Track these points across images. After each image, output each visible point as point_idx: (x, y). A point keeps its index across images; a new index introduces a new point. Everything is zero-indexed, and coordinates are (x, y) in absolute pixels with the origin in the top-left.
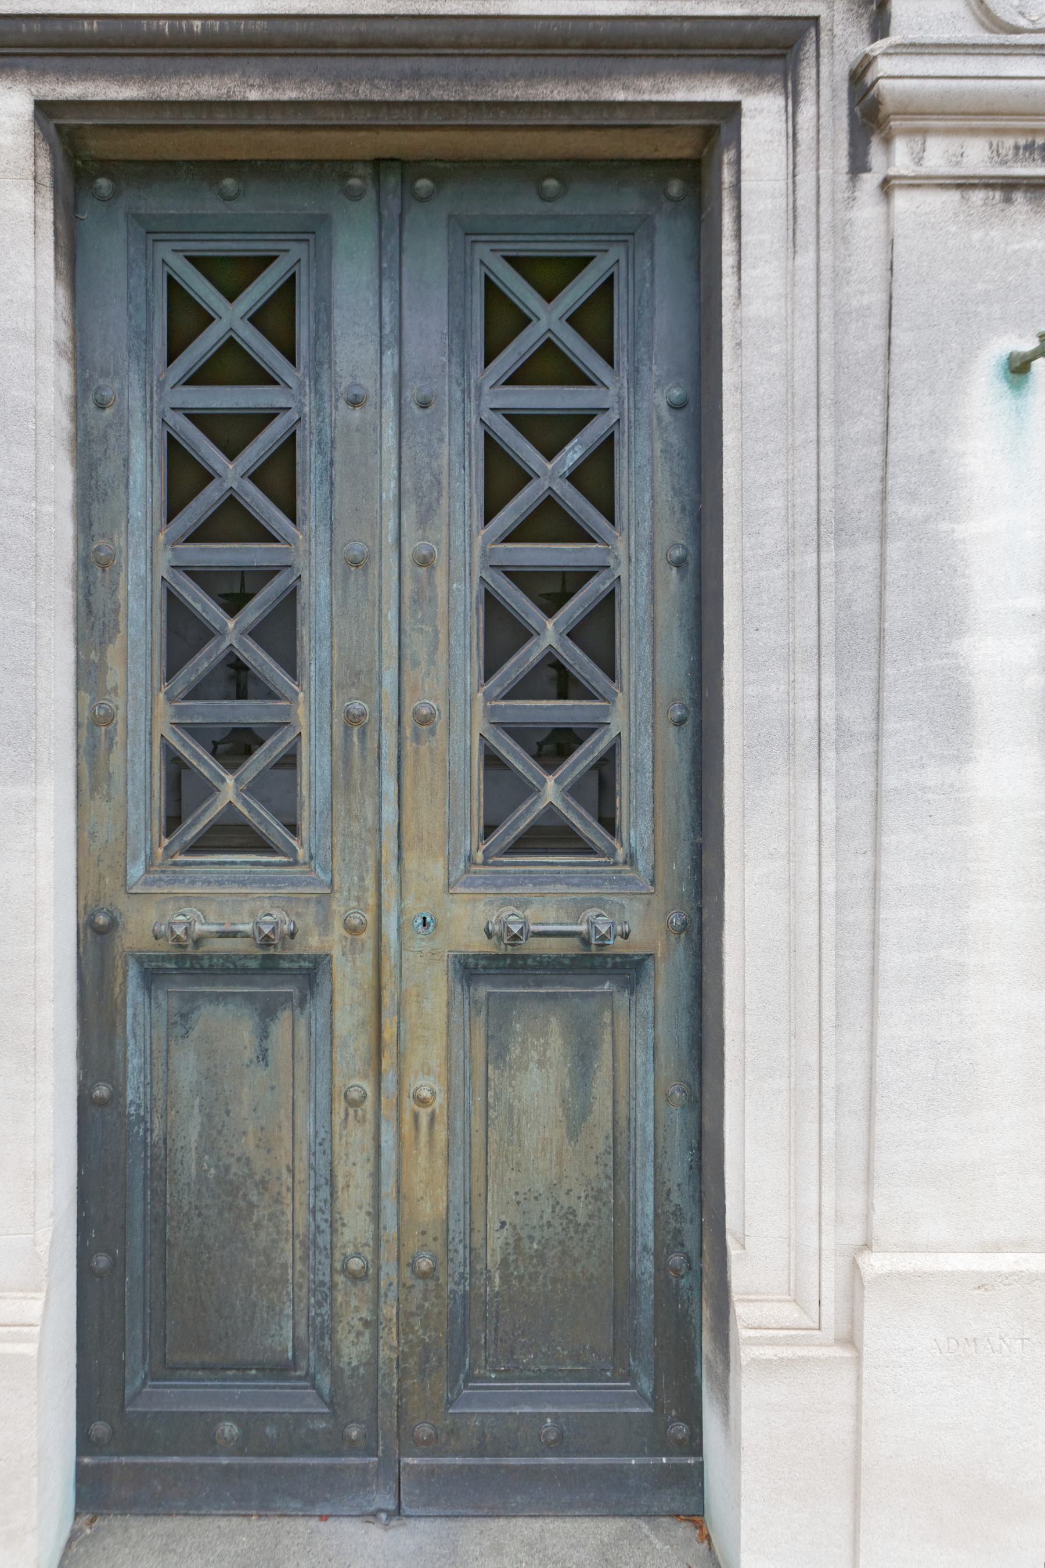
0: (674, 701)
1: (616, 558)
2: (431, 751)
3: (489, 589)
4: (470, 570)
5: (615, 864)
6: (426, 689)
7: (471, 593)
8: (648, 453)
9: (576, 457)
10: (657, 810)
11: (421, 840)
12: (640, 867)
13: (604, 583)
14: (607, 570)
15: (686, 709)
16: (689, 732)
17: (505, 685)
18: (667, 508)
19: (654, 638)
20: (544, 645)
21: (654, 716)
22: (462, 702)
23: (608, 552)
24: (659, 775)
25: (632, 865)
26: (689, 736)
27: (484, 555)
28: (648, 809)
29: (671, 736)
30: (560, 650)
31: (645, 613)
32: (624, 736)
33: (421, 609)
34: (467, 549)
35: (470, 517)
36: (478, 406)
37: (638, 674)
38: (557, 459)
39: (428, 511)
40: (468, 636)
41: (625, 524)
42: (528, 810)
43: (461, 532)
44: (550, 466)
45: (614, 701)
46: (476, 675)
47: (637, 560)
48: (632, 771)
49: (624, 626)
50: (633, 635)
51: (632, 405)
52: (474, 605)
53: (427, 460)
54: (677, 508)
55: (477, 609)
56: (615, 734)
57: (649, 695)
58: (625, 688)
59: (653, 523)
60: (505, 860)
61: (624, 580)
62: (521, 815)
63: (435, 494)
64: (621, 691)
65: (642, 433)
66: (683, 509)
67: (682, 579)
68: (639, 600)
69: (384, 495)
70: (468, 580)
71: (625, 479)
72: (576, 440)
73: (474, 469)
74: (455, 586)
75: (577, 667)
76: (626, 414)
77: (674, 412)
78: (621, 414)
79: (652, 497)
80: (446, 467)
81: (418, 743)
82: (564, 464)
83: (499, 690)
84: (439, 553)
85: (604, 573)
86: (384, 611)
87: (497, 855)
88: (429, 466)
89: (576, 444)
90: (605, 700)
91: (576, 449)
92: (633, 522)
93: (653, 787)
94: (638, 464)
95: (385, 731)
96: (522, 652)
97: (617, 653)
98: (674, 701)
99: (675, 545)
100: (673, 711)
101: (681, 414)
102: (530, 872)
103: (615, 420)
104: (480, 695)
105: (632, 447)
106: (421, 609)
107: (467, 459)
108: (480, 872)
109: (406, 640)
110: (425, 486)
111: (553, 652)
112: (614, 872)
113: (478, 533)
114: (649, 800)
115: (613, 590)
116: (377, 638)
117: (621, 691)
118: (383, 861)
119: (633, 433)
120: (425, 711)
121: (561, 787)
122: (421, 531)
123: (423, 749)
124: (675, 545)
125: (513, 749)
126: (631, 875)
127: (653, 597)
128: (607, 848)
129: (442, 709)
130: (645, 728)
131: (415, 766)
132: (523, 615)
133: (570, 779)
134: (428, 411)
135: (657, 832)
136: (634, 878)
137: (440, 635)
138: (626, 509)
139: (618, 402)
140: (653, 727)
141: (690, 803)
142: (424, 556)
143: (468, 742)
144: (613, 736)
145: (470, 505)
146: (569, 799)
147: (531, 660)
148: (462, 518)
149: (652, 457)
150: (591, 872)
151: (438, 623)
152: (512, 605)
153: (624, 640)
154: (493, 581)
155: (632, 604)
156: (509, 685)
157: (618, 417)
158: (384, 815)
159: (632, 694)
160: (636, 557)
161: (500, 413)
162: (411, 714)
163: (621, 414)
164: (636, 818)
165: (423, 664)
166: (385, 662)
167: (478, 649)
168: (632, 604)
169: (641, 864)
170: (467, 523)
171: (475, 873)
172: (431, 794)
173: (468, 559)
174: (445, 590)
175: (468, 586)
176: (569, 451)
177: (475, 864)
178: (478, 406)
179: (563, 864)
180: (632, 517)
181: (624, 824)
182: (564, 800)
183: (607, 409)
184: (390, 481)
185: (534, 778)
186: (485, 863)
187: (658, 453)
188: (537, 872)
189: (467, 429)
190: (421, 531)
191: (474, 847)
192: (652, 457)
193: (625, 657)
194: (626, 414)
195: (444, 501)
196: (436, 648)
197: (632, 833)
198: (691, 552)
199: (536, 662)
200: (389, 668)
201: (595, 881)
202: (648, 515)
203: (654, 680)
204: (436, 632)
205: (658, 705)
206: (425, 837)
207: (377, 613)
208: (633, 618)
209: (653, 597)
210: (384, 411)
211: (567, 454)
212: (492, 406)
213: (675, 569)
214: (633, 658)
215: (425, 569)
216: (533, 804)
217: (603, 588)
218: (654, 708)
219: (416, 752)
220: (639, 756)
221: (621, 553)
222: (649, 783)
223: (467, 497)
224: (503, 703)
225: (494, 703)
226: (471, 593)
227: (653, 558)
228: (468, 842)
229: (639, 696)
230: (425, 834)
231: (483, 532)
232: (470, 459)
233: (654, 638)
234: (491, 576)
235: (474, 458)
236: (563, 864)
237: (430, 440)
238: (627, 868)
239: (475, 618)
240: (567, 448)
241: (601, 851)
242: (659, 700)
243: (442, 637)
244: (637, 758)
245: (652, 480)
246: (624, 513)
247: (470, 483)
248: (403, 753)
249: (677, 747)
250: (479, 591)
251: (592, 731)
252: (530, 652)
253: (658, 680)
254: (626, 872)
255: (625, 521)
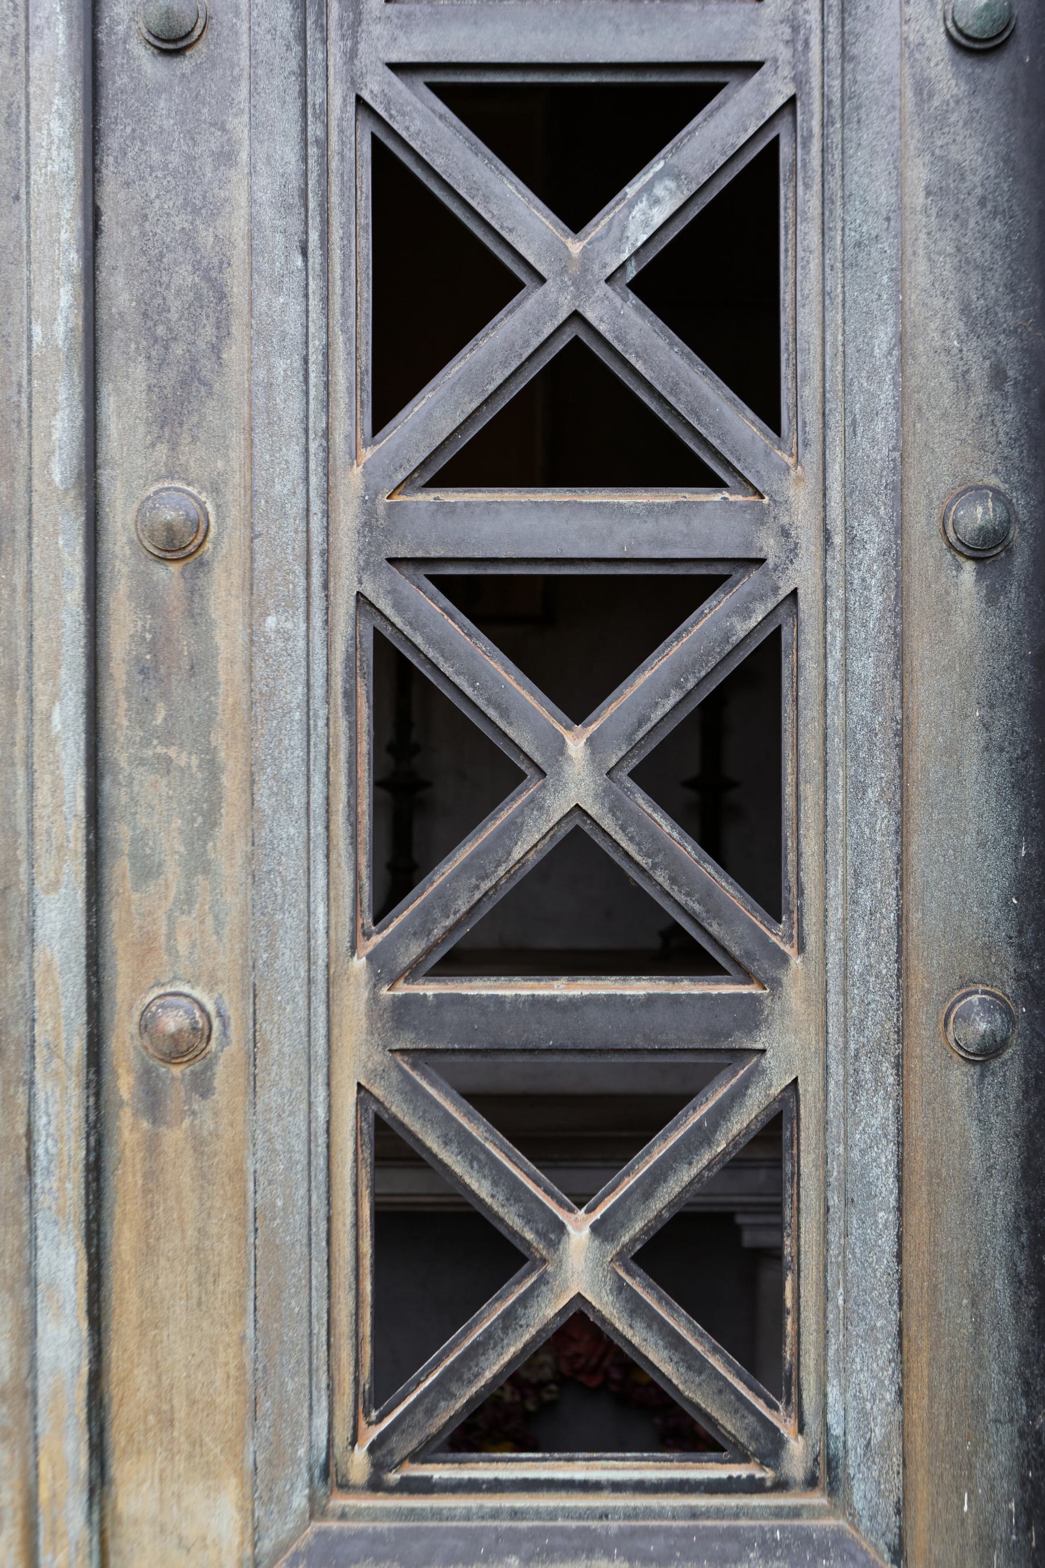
0: (966, 984)
1: (785, 533)
2: (199, 1144)
3: (387, 632)
4: (326, 573)
5: (781, 1486)
6: (183, 946)
7: (328, 644)
8: (885, 197)
9: (659, 216)
10: (913, 1328)
11: (168, 1422)
12: (858, 1501)
13: (745, 613)
14: (755, 574)
15: (1007, 1012)
16: (1015, 1083)
17: (437, 932)
18: (944, 374)
19: (903, 788)
20: (559, 806)
21: (901, 1033)
22: (299, 987)
23: (761, 516)
24: (916, 1217)
25: (832, 1491)
26: (1014, 1094)
27: (368, 525)
28: (885, 1322)
29: (955, 1095)
30: (608, 824)
31: (875, 707)
32: (808, 1090)
33: (165, 695)
34: (316, 506)
35: (327, 405)
36: (351, 55)
37: (851, 900)
38: (599, 225)
39: (184, 383)
40: (318, 780)
41: (814, 430)
42: (509, 1319)
43: (293, 454)
44: (575, 246)
45: (775, 984)
46: (347, 902)
47: (851, 539)
48: (834, 1200)
49: (810, 745)
50: (838, 777)
51: (834, 49)
52: (338, 684)
53: (181, 221)
54: (980, 374)
55: (350, 695)
56: (778, 1084)
57: (887, 967)
58: (812, 941)
59: (902, 421)
60: (439, 1472)
61: (807, 603)
62: (488, 1334)
63: (209, 332)
64: (801, 949)
65: (866, 136)
66: (998, 377)
67: (992, 597)
68: (856, 667)
69: (37, 330)
70: (317, 603)
71: (810, 285)
72: (657, 165)
73: (337, 255)
74: (271, 622)
75: (660, 877)
76: (815, 81)
77: (967, 64)
78: (800, 80)
79: (901, 339)
80: (242, 245)
81: (155, 1121)
82: (622, 238)
83: (415, 949)
84: (221, 517)
85: (748, 582)
86: (41, 703)
87: (417, 1456)
88: (188, 240)
89: (659, 176)
90: (748, 977)
91: (659, 191)
92: (835, 419)
93: (899, 1257)
94: (852, 236)
95: (44, 1087)
96: (491, 827)
97: (788, 831)
98: (966, 984)
99: (975, 491)
100: (964, 1017)
101: (992, 72)
102: (515, 1514)
103: (780, 101)
104: (359, 963)
105: (834, 183)
106: (165, 695)
107: (315, 222)
108: (359, 1514)
109: (114, 793)
110: (175, 305)
111: (587, 828)
112: (778, 1513)
113: (354, 456)
114: (887, 1296)
115: (776, 636)
116: (21, 790)
117: (801, 949)
118: (44, 1494)
119: (837, 138)
120: (172, 1022)
121: (612, 1250)
122: (162, 449)
123: (174, 1137)
124: (975, 491)
125: (461, 1130)
126: (830, 1522)
127: (900, 658)
128: (754, 1437)
129: (231, 1013)
130: (875, 1070)
131: (146, 1191)
132: (492, 713)
133: (638, 1226)
134: (185, 65)
135: (913, 1395)
136: (839, 1537)
137: (225, 780)
138: (816, 381)
139: (791, 42)
140: (899, 1066)
141: (1016, 1305)
142: (169, 528)
143: (321, 1112)
144: (775, 1091)
145: (327, 369)
146: (636, 1284)
147: (517, 854)
148: (295, 407)
149: (900, 207)
150: (706, 1514)
151: (217, 739)
152: (458, 680)
153: (810, 792)
154: (396, 606)
155: (834, 677)
156: (450, 931)
157: (789, 91)
158: (45, 1352)
159: (834, 960)
160: (848, 529)
161: (419, 81)
162: (134, 1029)
163: (800, 80)
164: (847, 1348)
165: (173, 873)
166: (46, 866)
167: (354, 823)
168: (834, 677)
169: (860, 1493)
170: (317, 423)
171: (343, 1516)
172: (200, 1279)
173: (317, 538)
174: (242, 638)
175: (317, 620)
176: (638, 196)
177: (345, 1486)
178: (351, 55)
179: (617, 1487)
180: (835, 405)
181: (809, 1361)
182: (620, 1288)
183: (756, 66)
184: (55, 284)
185: (528, 1221)
186: (375, 1485)
187: (919, 200)
188: (538, 1514)
189: (315, 129)
190: (162, 449)
191: (343, 1434)
192: (900, 207)
193: (810, 846)
194: (815, 81)
195: (234, 353)
196: (211, 818)
197: (833, 1392)
198: (1023, 513)
199: (534, 858)
200: (54, 885)
201: (716, 1546)
202: (886, 394)
203: (901, 919)
204: (212, 768)
205: (915, 998)
206: (181, 1414)
207: (21, 708)
208: (836, 720)
209: (900, 658)
210: (36, 57)
211: (631, 206)
212: (395, 57)
213: (969, 566)
214: (837, 849)
215: (175, 568)
216: (524, 1300)
217: (742, 628)
218: (903, 1007)
219: (152, 1146)
220: (855, 1155)
221: (800, 519)
222: (887, 1243)
223: (316, 344)
224: (430, 989)
225: (403, 989)
226: (328, 644)
227: (900, 531)
228: (321, 1421)
229: (857, 967)
230: (179, 1402)
231: (367, 454)
232: (326, 222)
233: (903, 788)
234: (392, 592)
235: (337, 219)
236: (617, 1487)
237: (190, 159)
238: (818, 1499)
239: (342, 725)
240: (630, 190)
241: (736, 1444)
242: (918, 981)
243: (230, 783)
244: (847, 1164)
245: (899, 285)
246: (810, 392)
247: (326, 300)
248: (111, 1152)
249: (974, 1131)
250: (355, 640)
251: (708, 1076)
252: (513, 828)
253: (915, 918)
254: (815, 1512)
255: (811, 415)
